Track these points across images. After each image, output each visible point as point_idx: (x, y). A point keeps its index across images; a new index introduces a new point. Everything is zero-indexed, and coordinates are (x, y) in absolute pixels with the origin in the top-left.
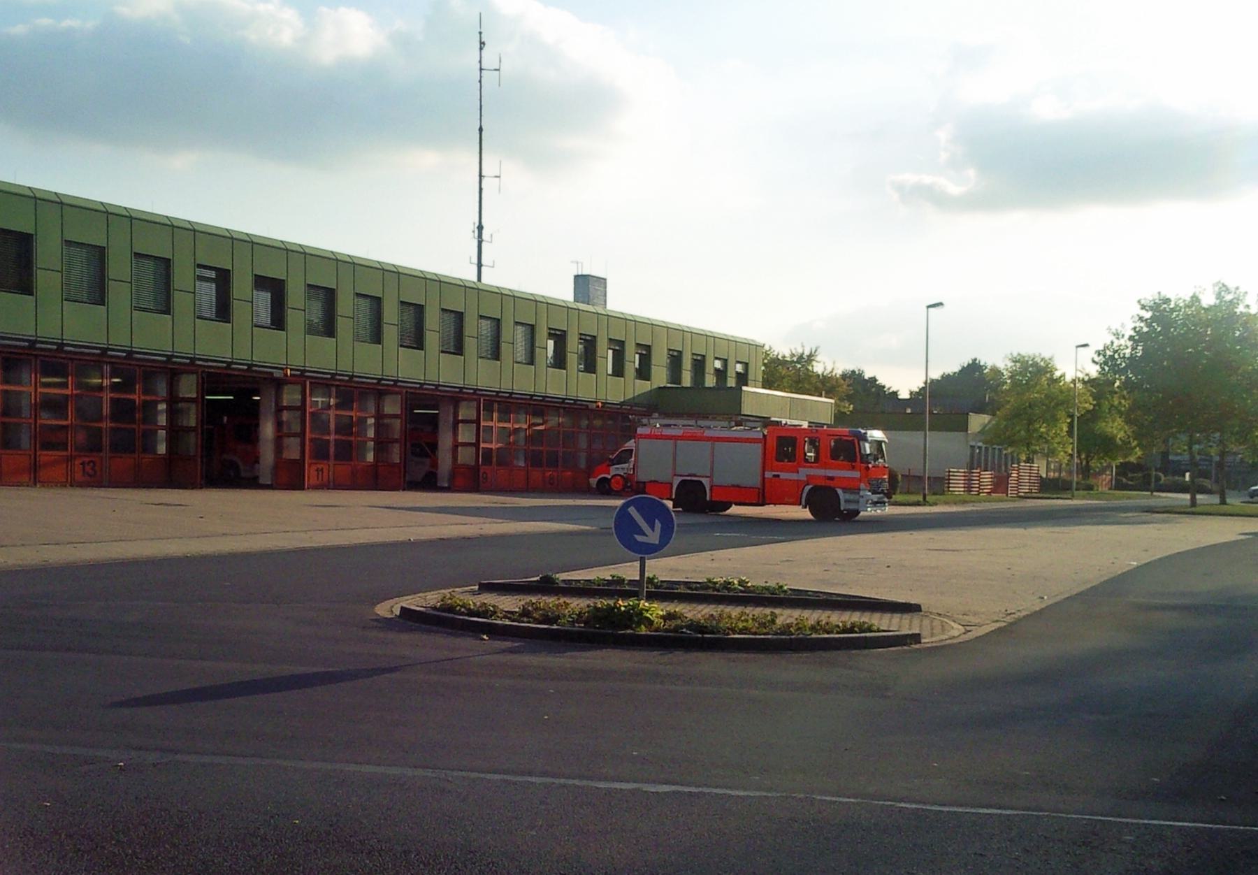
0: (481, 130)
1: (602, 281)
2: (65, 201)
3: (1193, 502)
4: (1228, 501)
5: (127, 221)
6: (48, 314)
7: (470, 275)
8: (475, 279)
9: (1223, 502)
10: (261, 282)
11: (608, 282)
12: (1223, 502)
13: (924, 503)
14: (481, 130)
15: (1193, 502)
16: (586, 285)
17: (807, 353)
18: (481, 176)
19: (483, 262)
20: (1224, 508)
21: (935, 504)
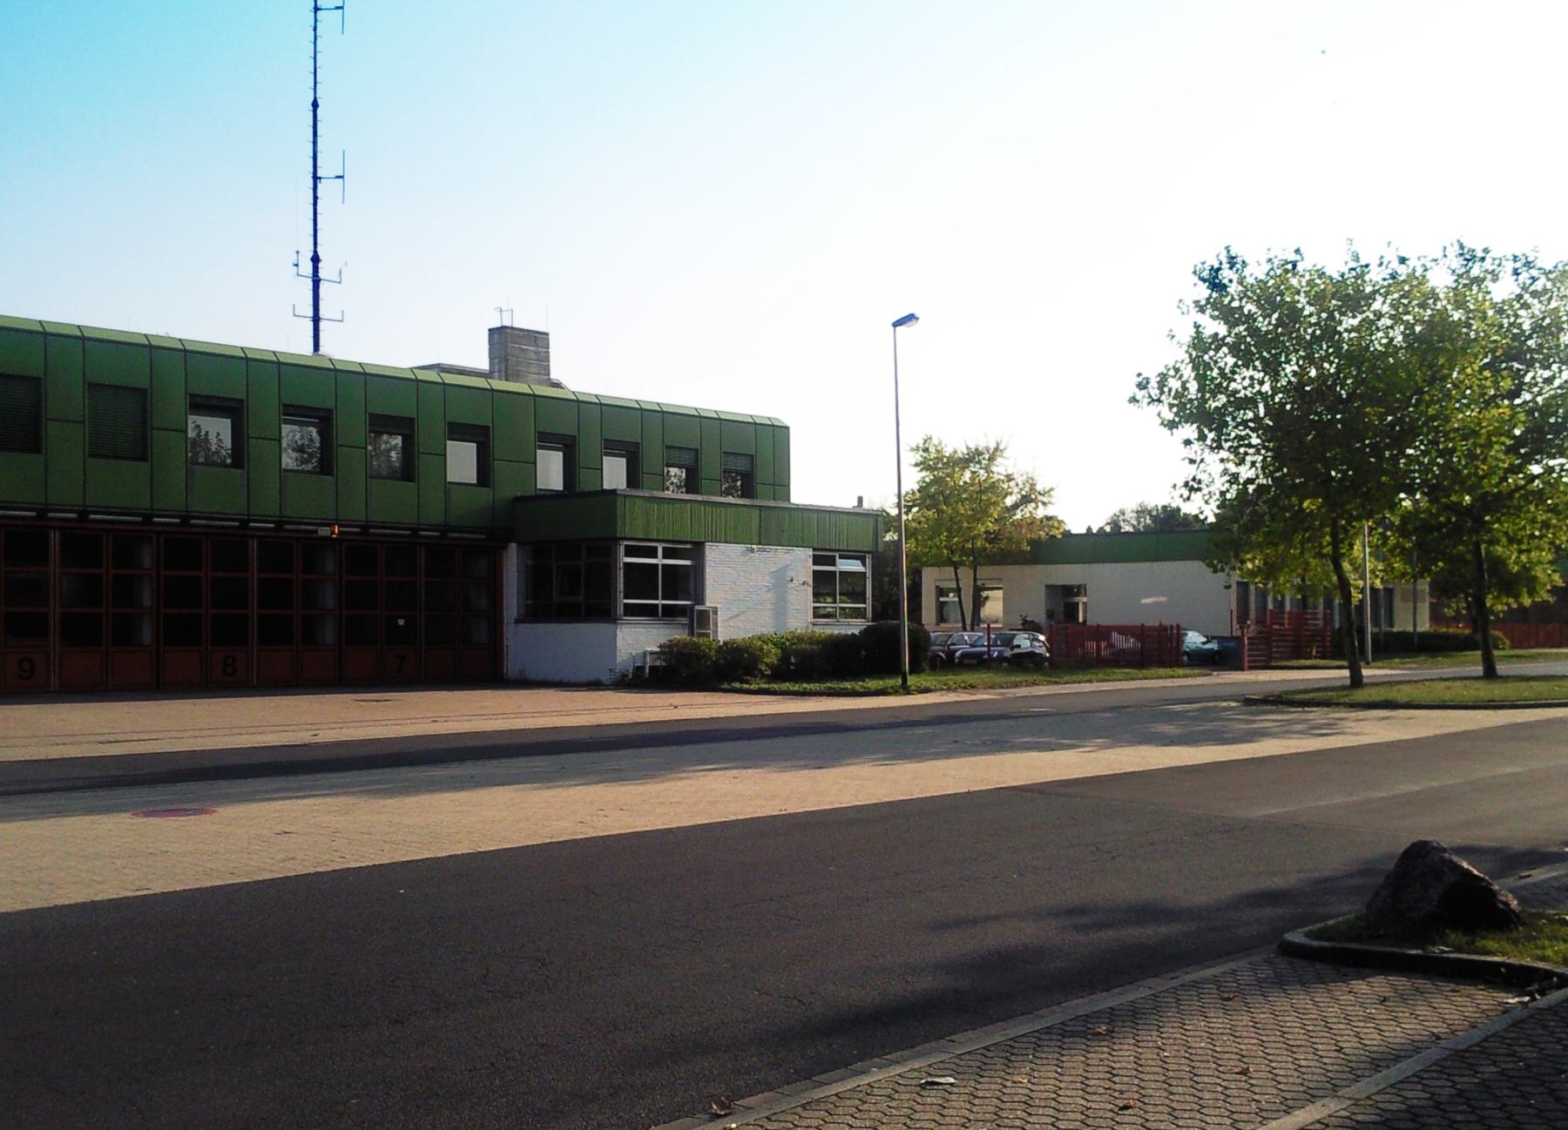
0: (315, 105)
1: (539, 339)
2: (49, 329)
3: (1357, 681)
4: (1501, 668)
5: (332, 374)
6: (68, 477)
7: (292, 342)
8: (306, 348)
9: (1490, 674)
10: (381, 424)
11: (551, 337)
12: (1490, 674)
13: (906, 690)
14: (315, 105)
15: (1357, 681)
16: (503, 340)
17: (992, 446)
18: (316, 178)
19: (322, 313)
20: (1360, 695)
21: (926, 691)
